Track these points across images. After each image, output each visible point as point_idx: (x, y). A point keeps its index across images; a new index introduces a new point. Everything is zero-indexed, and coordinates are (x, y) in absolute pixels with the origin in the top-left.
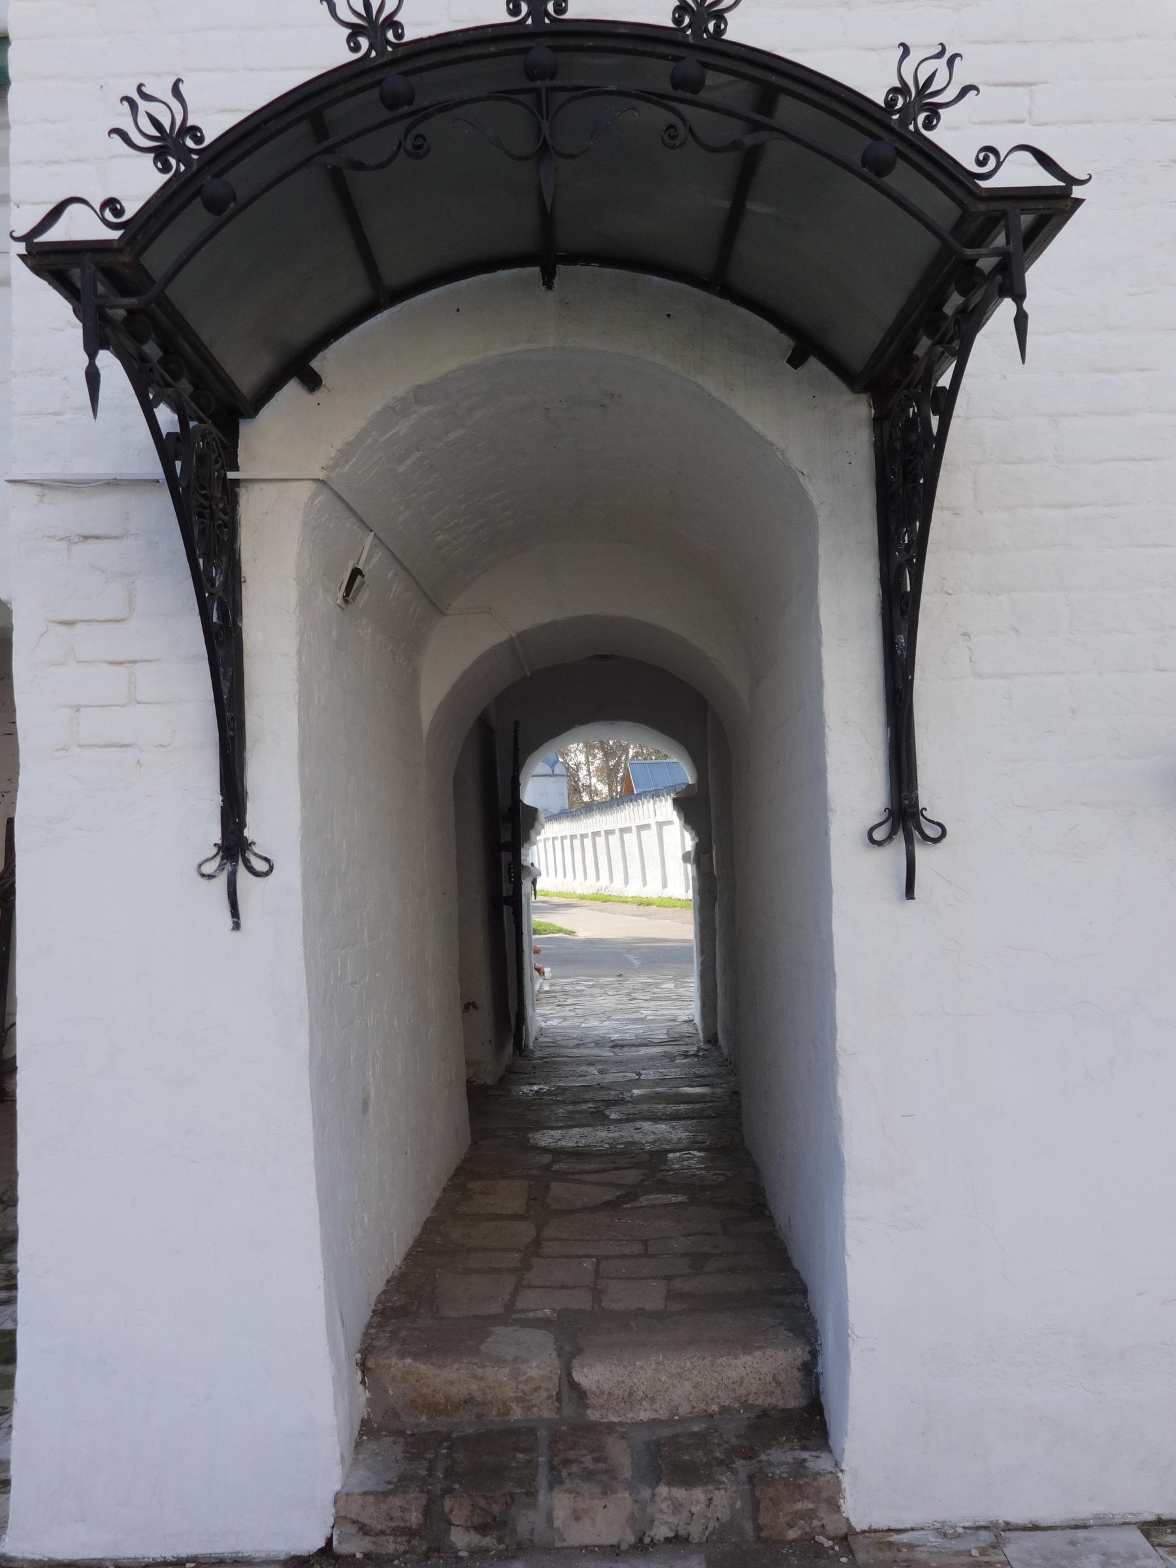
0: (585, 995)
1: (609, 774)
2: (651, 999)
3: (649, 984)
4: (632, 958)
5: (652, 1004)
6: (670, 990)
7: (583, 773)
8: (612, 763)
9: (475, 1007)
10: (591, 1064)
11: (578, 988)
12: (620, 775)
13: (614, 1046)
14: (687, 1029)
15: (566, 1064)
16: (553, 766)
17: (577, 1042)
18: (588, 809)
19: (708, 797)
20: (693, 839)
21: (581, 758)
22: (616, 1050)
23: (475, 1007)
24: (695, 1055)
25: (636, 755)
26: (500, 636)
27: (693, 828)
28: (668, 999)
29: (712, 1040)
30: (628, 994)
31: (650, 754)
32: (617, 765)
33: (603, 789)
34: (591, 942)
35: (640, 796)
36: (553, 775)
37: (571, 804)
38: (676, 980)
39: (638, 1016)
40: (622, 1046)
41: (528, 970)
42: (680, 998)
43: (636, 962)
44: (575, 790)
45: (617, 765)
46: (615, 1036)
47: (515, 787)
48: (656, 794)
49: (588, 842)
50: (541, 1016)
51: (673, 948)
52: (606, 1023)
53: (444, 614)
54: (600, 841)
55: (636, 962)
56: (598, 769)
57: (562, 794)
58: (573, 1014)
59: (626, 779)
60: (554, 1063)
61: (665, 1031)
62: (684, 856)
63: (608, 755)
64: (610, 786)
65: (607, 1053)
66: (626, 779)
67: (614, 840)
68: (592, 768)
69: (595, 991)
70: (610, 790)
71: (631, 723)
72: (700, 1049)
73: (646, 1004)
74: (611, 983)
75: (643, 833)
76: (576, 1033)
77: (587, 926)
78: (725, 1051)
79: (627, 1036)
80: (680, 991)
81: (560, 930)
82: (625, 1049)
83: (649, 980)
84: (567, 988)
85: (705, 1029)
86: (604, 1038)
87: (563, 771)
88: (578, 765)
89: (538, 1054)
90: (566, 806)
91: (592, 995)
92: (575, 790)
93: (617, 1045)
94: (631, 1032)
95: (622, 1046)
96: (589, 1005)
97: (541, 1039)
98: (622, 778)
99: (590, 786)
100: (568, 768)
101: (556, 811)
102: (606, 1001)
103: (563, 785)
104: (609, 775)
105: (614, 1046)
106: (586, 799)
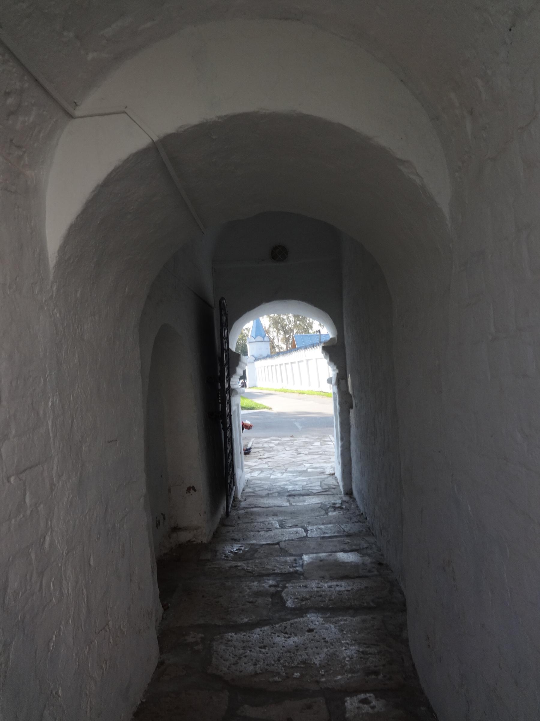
0: (274, 451)
1: (286, 340)
2: (309, 454)
3: (306, 443)
4: (297, 424)
5: (310, 457)
6: (318, 448)
7: (276, 341)
8: (287, 336)
9: (195, 490)
10: (275, 514)
11: (271, 445)
12: (291, 341)
13: (290, 496)
14: (331, 481)
15: (259, 514)
16: (264, 338)
17: (267, 492)
18: (278, 354)
19: (344, 345)
20: (334, 370)
21: (275, 334)
22: (291, 499)
23: (195, 490)
24: (341, 508)
25: (297, 333)
26: (141, 142)
27: (335, 364)
28: (317, 453)
29: (349, 493)
30: (297, 450)
31: (302, 332)
32: (290, 336)
33: (284, 347)
34: (279, 414)
35: (298, 349)
36: (264, 341)
37: (271, 353)
38: (320, 439)
39: (302, 468)
40: (295, 495)
41: (238, 450)
42: (324, 453)
43: (300, 427)
44: (273, 347)
45: (290, 336)
46: (290, 488)
47: (225, 339)
48: (313, 346)
49: (278, 367)
50: (250, 467)
51: (316, 418)
52: (285, 475)
53: (71, 117)
54: (283, 367)
55: (300, 427)
56: (282, 339)
57: (267, 349)
58: (266, 466)
59: (293, 342)
60: (252, 513)
61: (319, 484)
62: (328, 380)
63: (285, 333)
64: (287, 345)
65: (283, 502)
66: (293, 342)
67: (289, 366)
68: (280, 338)
69: (280, 448)
70: (287, 347)
71: (296, 302)
72: (343, 502)
73: (306, 458)
74: (288, 441)
75: (300, 363)
76: (267, 485)
77: (278, 405)
78: (361, 508)
79: (297, 488)
80: (324, 447)
81: (265, 408)
82: (296, 498)
83: (307, 440)
84: (266, 445)
85: (344, 486)
86: (283, 489)
87: (268, 340)
88: (274, 337)
89: (243, 504)
90: (269, 354)
91: (278, 451)
92: (273, 347)
93: (291, 495)
94: (300, 483)
95: (295, 495)
96: (276, 458)
97: (248, 490)
98: (291, 342)
99: (279, 346)
100: (270, 339)
101: (265, 355)
102: (284, 455)
103: (268, 345)
104: (286, 341)
105: (290, 496)
106: (277, 350)
